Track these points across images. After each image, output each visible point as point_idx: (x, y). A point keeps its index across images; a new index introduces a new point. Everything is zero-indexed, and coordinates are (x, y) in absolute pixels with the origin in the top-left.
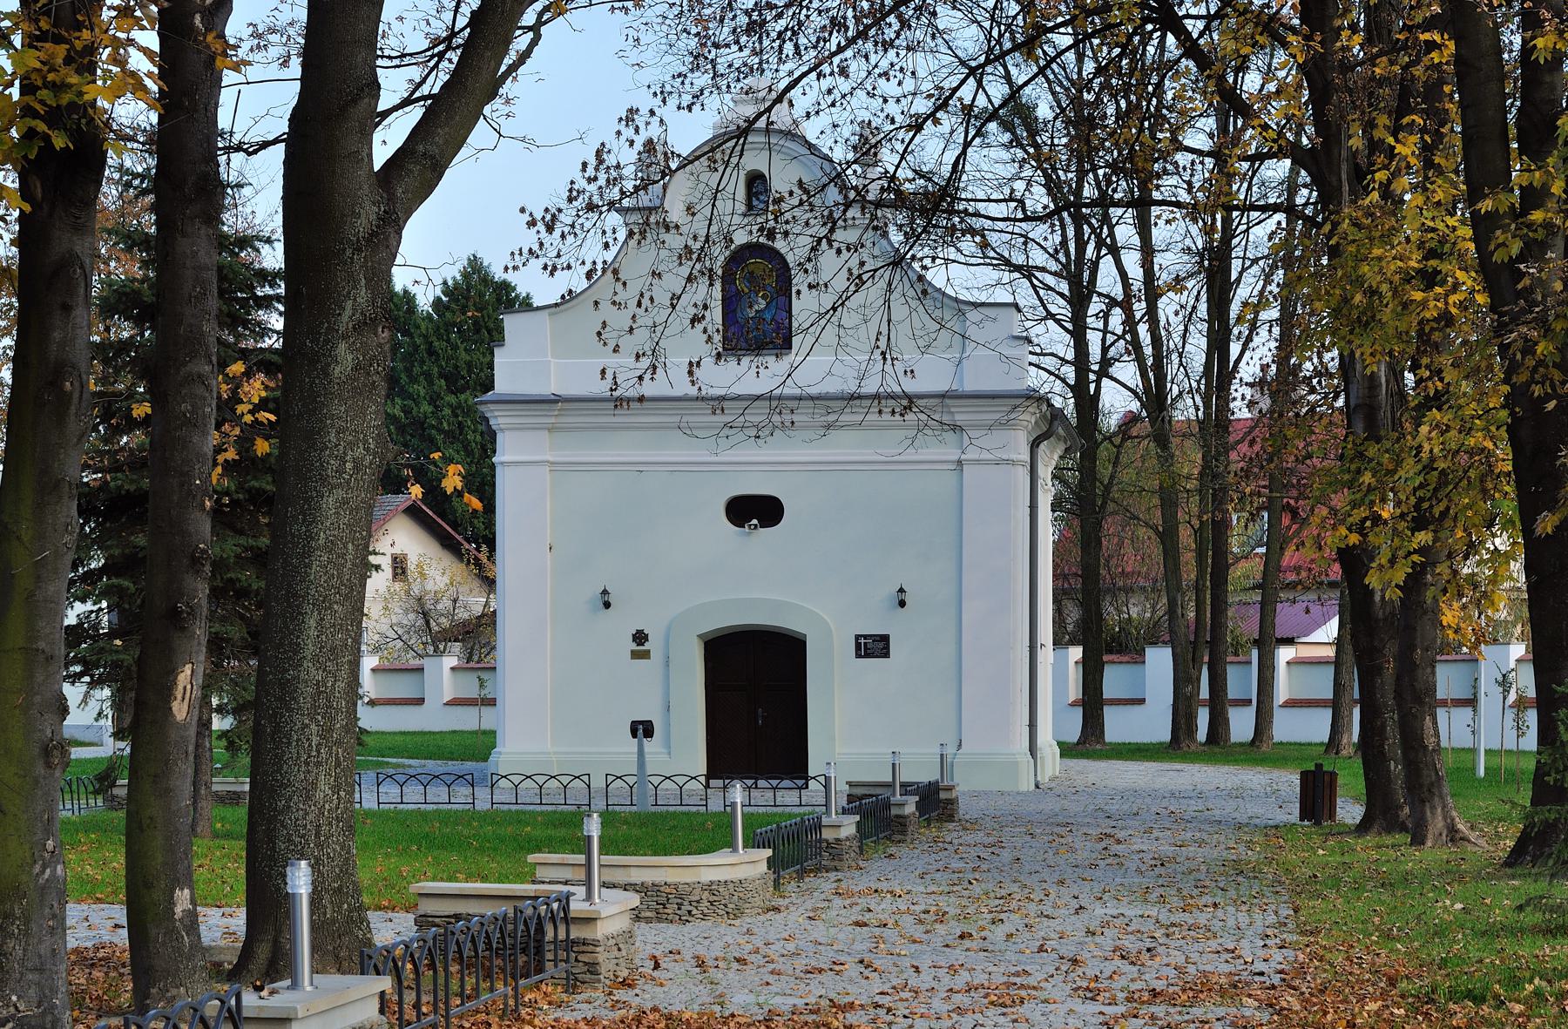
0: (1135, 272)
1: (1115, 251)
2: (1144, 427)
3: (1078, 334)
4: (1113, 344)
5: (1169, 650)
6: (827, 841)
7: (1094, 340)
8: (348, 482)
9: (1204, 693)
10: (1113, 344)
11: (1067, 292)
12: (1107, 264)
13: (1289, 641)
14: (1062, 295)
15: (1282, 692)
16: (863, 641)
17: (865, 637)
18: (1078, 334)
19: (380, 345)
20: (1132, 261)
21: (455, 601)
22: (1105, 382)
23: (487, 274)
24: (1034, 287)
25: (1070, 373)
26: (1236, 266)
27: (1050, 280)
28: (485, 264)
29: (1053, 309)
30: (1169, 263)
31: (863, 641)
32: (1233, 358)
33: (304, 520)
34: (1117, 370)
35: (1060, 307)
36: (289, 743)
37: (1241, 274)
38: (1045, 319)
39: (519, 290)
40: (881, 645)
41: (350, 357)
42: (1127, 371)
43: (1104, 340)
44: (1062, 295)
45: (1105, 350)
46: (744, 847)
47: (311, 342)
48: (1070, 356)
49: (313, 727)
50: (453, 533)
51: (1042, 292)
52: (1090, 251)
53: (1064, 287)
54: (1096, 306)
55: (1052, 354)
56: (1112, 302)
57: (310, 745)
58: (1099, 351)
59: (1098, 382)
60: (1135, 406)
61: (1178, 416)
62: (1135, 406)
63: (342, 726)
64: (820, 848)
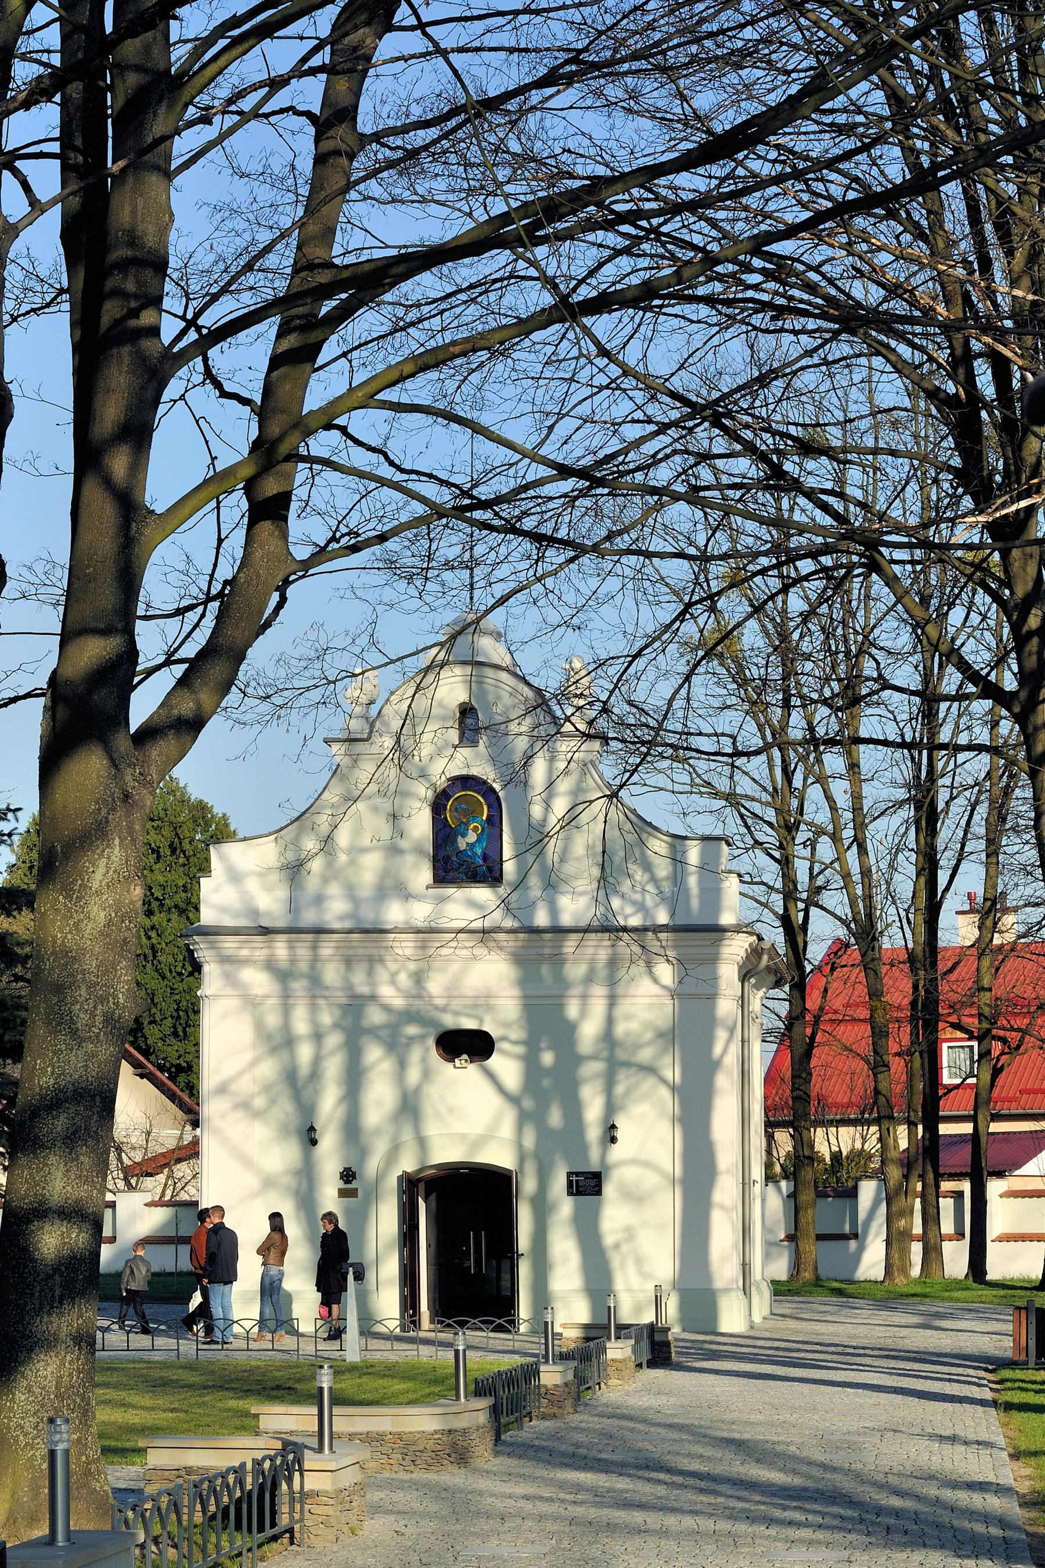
0: (843, 801)
1: (822, 780)
2: (854, 953)
3: (785, 863)
4: (821, 872)
5: (177, 772)
6: (545, 1386)
7: (801, 870)
8: (98, 1036)
9: (918, 1229)
10: (821, 872)
11: (773, 820)
12: (815, 793)
13: (1000, 1174)
14: (770, 824)
15: (995, 1226)
16: (574, 1178)
17: (577, 1174)
18: (785, 863)
19: (132, 902)
20: (840, 789)
21: (148, 1133)
22: (814, 911)
23: (183, 795)
24: (742, 816)
25: (777, 902)
26: (943, 796)
27: (757, 808)
28: (182, 785)
29: (761, 837)
30: (874, 794)
31: (574, 1178)
32: (941, 887)
33: (52, 1073)
34: (828, 899)
35: (768, 836)
36: (32, 1294)
37: (947, 803)
38: (753, 847)
39: (215, 811)
40: (593, 1182)
41: (102, 914)
42: (835, 900)
43: (811, 869)
44: (770, 824)
45: (812, 877)
46: (466, 1397)
47: (65, 898)
48: (779, 885)
49: (57, 1277)
50: (145, 1062)
51: (750, 821)
52: (798, 781)
53: (770, 815)
54: (802, 836)
55: (763, 883)
56: (820, 832)
57: (53, 1296)
58: (807, 879)
59: (806, 911)
60: (842, 932)
61: (886, 943)
62: (842, 932)
63: (85, 1278)
64: (539, 1394)
